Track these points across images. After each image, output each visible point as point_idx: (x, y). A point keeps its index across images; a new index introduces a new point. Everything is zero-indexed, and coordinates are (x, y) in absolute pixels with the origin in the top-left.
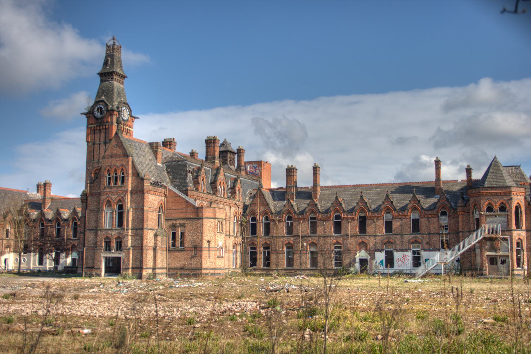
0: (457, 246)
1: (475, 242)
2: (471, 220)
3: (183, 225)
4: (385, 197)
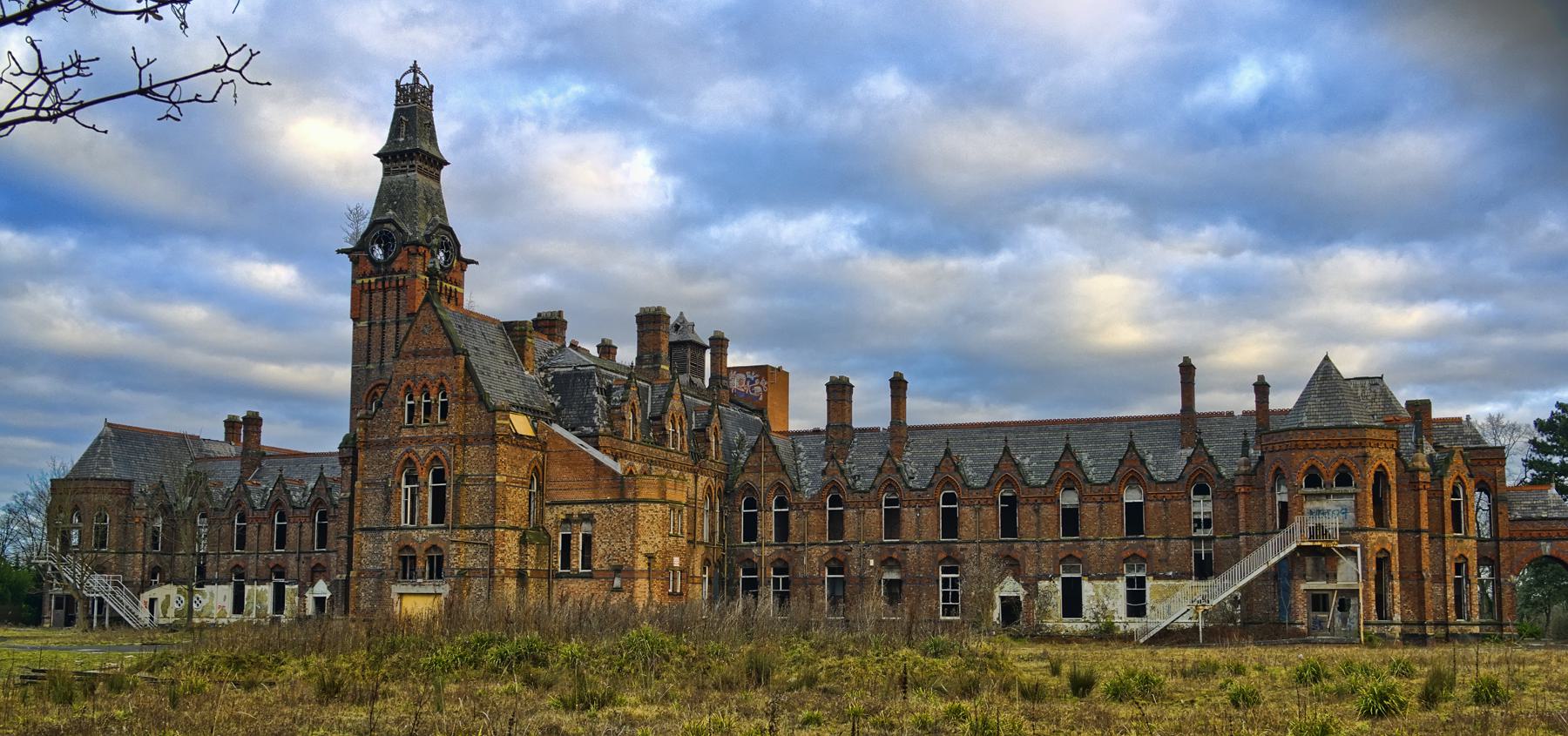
0: (1237, 568)
1: (1276, 559)
2: (1268, 507)
3: (589, 519)
4: (1061, 450)
